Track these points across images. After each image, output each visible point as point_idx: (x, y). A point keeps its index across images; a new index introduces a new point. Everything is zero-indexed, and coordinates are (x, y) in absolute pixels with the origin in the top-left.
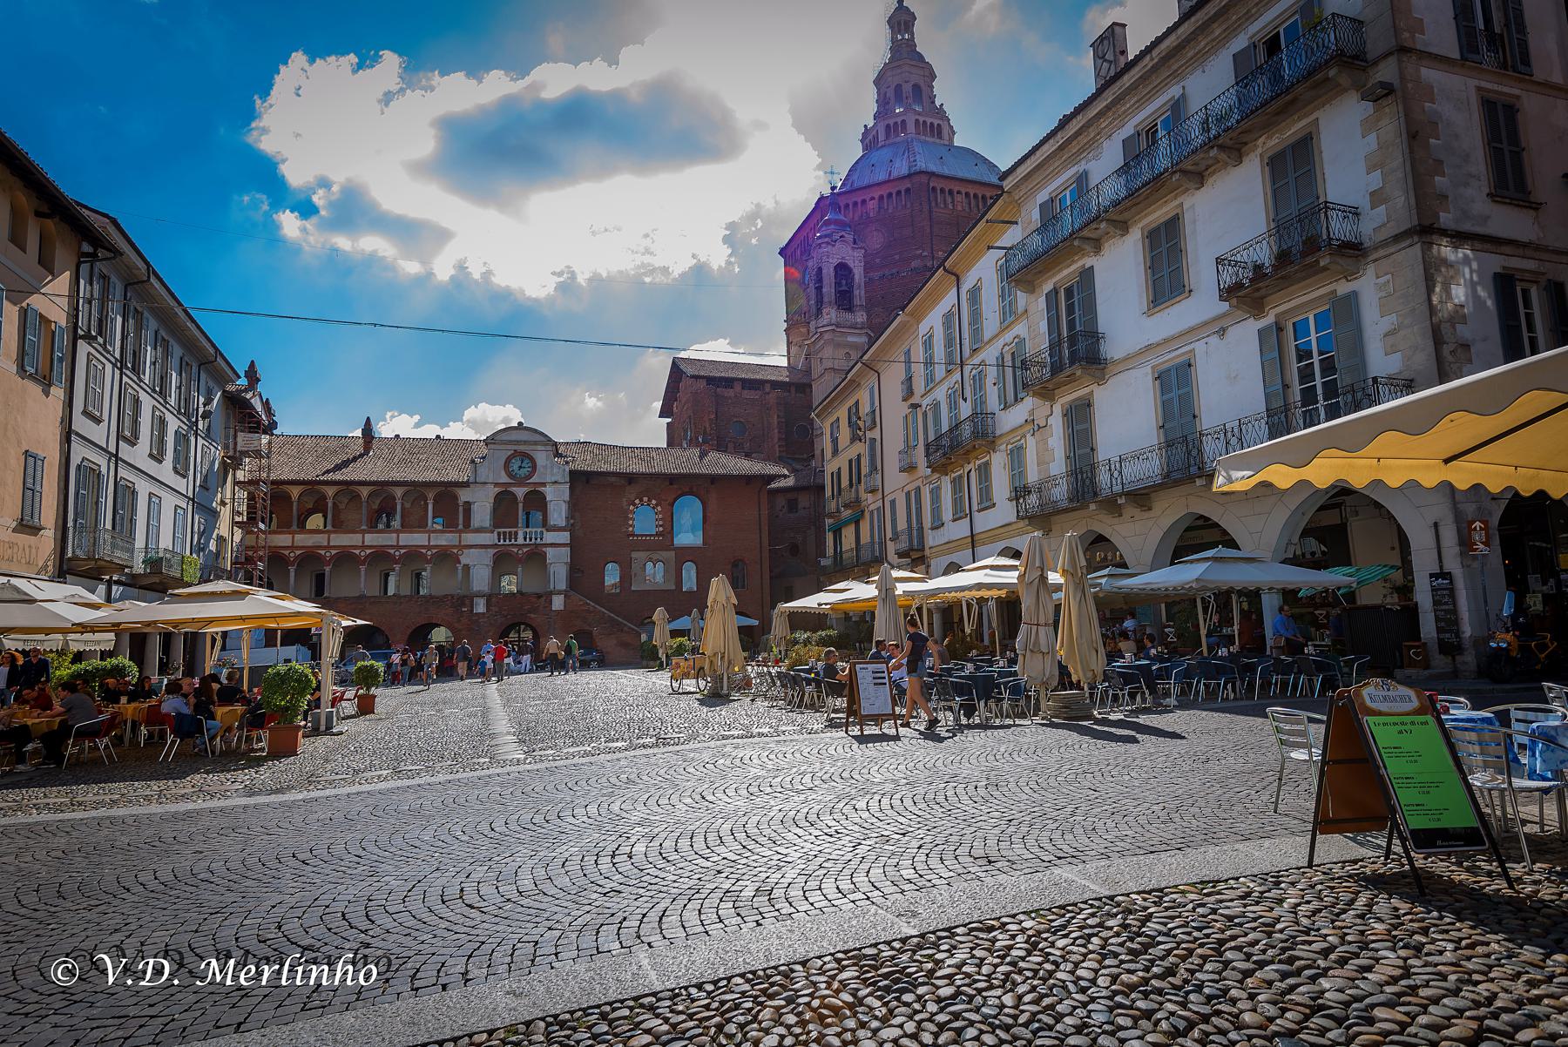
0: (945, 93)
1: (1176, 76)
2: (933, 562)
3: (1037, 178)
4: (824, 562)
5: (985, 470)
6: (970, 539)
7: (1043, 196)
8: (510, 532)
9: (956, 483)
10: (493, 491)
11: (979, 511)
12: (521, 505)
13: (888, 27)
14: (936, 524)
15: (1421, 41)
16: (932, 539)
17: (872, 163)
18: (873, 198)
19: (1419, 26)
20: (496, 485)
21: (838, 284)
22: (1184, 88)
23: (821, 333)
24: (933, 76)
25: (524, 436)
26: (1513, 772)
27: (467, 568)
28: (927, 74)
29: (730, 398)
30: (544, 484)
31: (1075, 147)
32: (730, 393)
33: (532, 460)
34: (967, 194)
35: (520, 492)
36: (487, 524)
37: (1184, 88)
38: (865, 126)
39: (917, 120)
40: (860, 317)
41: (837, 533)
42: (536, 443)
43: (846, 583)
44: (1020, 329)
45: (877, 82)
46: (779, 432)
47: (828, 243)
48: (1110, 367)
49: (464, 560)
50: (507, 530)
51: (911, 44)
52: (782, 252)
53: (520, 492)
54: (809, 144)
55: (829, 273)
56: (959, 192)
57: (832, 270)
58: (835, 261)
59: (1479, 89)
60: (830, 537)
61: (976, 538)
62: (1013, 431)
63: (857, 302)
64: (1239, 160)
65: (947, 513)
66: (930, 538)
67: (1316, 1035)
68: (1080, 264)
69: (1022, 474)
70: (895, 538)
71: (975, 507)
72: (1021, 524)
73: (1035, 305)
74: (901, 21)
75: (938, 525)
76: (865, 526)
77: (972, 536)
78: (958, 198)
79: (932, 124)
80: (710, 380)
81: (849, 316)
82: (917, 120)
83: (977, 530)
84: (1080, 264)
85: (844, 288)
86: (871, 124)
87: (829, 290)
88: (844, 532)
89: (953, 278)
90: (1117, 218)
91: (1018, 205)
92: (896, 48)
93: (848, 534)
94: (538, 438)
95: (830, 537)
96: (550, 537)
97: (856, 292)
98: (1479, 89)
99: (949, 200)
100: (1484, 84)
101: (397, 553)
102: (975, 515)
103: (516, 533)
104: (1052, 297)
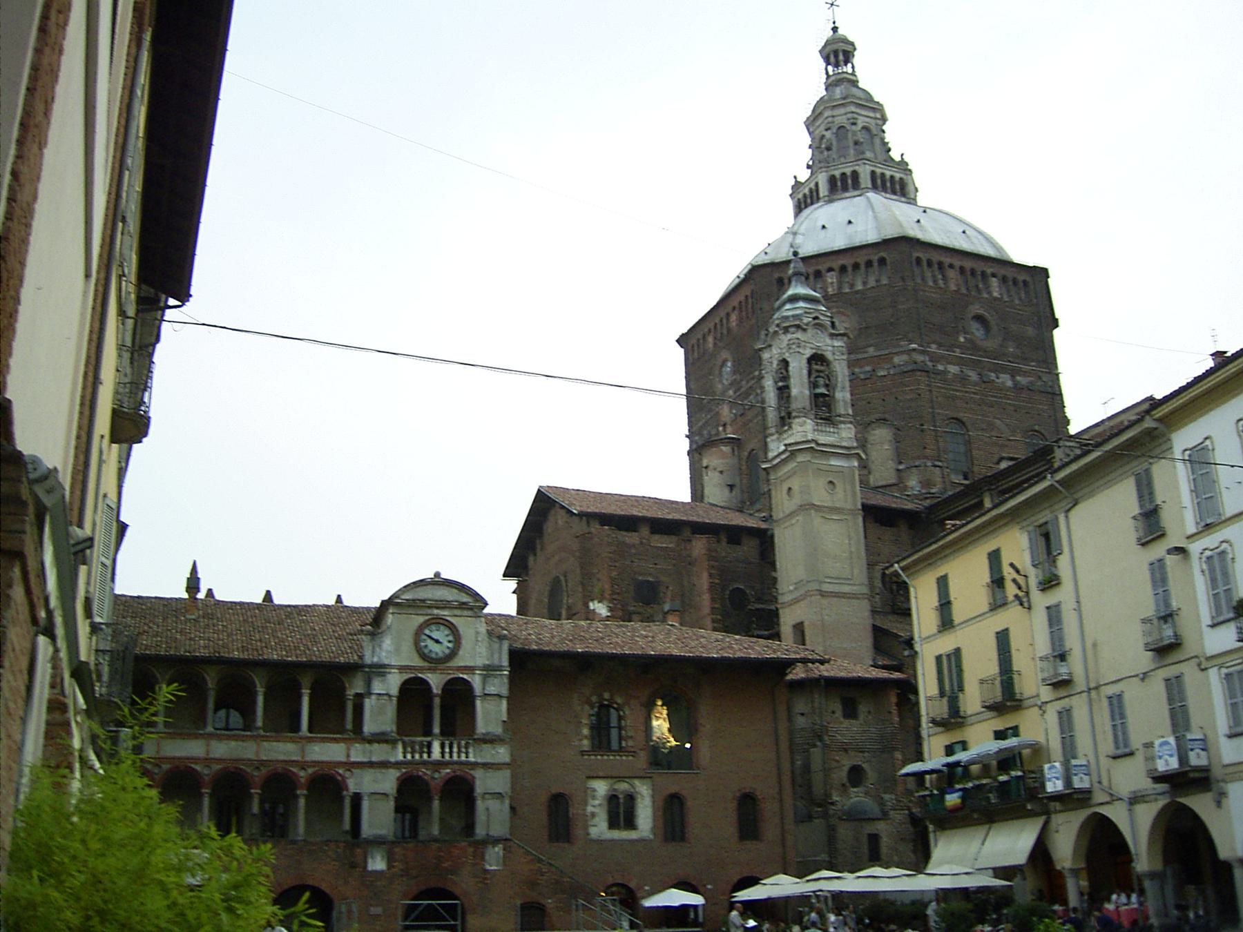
10: (393, 683)
12: (437, 701)
17: (820, 224)
18: (830, 270)
20: (402, 669)
24: (884, 119)
27: (357, 799)
28: (878, 116)
29: (634, 546)
30: (470, 669)
32: (631, 538)
34: (962, 269)
35: (436, 681)
36: (498, 730)
39: (873, 173)
40: (846, 434)
42: (462, 606)
43: (873, 869)
46: (713, 600)
47: (798, 327)
49: (352, 786)
52: (682, 340)
56: (951, 266)
58: (808, 353)
78: (951, 274)
79: (883, 175)
80: (606, 520)
82: (873, 173)
85: (822, 390)
86: (804, 175)
87: (799, 388)
94: (465, 598)
97: (839, 395)
99: (928, 274)
101: (437, 775)
103: (429, 745)
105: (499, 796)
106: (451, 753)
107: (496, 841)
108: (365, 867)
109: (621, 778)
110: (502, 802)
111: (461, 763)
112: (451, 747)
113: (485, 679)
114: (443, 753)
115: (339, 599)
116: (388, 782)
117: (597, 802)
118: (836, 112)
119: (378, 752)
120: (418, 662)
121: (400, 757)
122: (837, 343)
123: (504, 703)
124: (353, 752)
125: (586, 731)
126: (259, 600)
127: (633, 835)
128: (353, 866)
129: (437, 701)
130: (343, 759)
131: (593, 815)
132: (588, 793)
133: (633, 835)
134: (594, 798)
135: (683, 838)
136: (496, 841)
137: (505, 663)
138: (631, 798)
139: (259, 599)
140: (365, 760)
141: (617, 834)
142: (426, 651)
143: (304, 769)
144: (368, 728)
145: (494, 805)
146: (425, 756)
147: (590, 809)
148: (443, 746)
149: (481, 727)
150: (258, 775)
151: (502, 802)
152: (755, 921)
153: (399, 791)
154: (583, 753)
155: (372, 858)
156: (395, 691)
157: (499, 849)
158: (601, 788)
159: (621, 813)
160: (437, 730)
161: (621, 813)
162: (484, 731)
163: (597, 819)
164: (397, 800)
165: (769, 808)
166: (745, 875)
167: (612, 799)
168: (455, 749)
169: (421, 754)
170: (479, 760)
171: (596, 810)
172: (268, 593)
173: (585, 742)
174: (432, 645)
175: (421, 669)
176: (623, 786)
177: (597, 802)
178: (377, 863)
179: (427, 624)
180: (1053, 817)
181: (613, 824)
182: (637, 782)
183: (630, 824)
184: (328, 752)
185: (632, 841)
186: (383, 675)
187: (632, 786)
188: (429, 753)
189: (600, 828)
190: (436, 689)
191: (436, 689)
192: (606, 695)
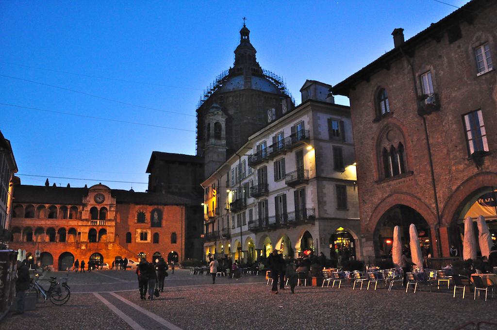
1: (282, 127)
2: (232, 239)
3: (257, 139)
4: (202, 236)
5: (244, 213)
7: (258, 144)
15: (320, 137)
16: (232, 232)
18: (230, 96)
19: (320, 133)
20: (91, 205)
21: (215, 130)
23: (209, 147)
26: (470, 114)
31: (263, 135)
33: (104, 199)
35: (99, 208)
51: (248, 41)
53: (99, 208)
54: (197, 135)
59: (333, 146)
60: (205, 227)
63: (222, 136)
64: (291, 152)
65: (236, 225)
66: (232, 231)
68: (264, 164)
69: (252, 218)
70: (223, 230)
74: (245, 32)
75: (234, 228)
76: (216, 224)
77: (241, 232)
81: (219, 141)
84: (264, 164)
85: (218, 131)
92: (242, 41)
93: (210, 227)
94: (106, 188)
95: (205, 227)
96: (108, 224)
98: (333, 146)
100: (334, 145)
102: (242, 226)
104: (259, 171)
105: (112, 233)
107: (111, 243)
109: (144, 229)
113: (110, 207)
115: (69, 185)
116: (87, 230)
118: (249, 50)
119: (85, 223)
121: (90, 224)
125: (136, 218)
127: (146, 242)
128: (78, 248)
131: (137, 237)
133: (146, 242)
135: (158, 243)
136: (111, 243)
137: (115, 203)
138: (146, 234)
139: (84, 187)
141: (142, 241)
144: (83, 217)
145: (111, 235)
150: (67, 228)
152: (352, 164)
153: (89, 231)
155: (348, 178)
156: (89, 210)
157: (112, 244)
158: (139, 231)
159: (144, 236)
161: (144, 236)
163: (138, 238)
165: (179, 236)
167: (142, 234)
172: (69, 184)
174: (98, 199)
175: (95, 205)
176: (145, 231)
178: (83, 248)
179: (97, 195)
181: (142, 239)
182: (148, 230)
183: (146, 239)
184: (73, 223)
189: (138, 240)
191: (99, 210)
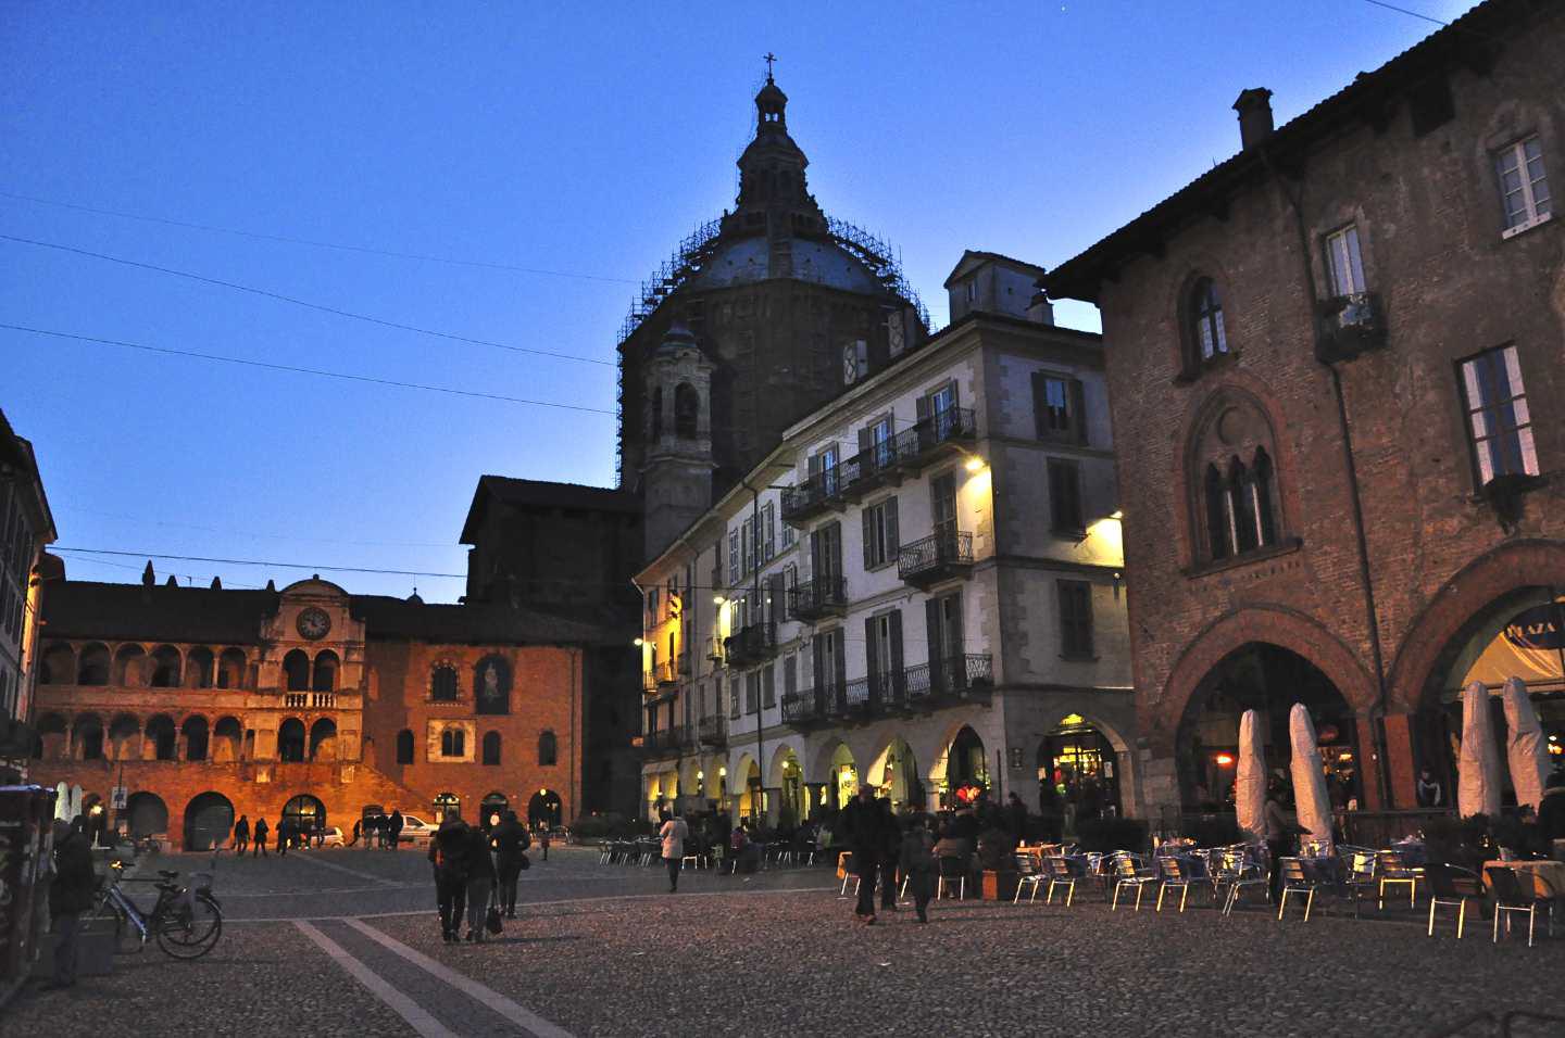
0: (818, 185)
1: (888, 398)
3: (809, 436)
4: (636, 742)
5: (770, 670)
6: (757, 734)
7: (812, 451)
8: (299, 696)
9: (750, 677)
11: (766, 708)
12: (312, 665)
13: (755, 105)
14: (735, 715)
16: (732, 729)
19: (1007, 419)
20: (286, 643)
22: (893, 408)
24: (805, 163)
25: (318, 590)
31: (829, 424)
35: (311, 653)
37: (893, 408)
38: (726, 211)
41: (653, 707)
44: (794, 557)
45: (740, 163)
48: (850, 609)
49: (248, 725)
50: (296, 693)
51: (781, 127)
53: (311, 653)
55: (668, 394)
57: (673, 391)
58: (677, 382)
59: (1048, 458)
61: (763, 732)
62: (788, 643)
63: (700, 428)
64: (918, 477)
65: (744, 709)
67: (303, 595)
70: (703, 722)
71: (762, 705)
72: (784, 727)
73: (803, 538)
74: (771, 101)
75: (736, 717)
76: (679, 705)
77: (760, 730)
83: (764, 726)
84: (831, 517)
85: (686, 413)
88: (659, 709)
89: (752, 493)
90: (856, 491)
91: (795, 451)
92: (763, 128)
95: (646, 713)
98: (1048, 458)
100: (1053, 454)
103: (305, 696)
105: (354, 732)
106: (320, 702)
108: (255, 780)
109: (454, 719)
110: (356, 736)
111: (326, 709)
112: (321, 698)
113: (347, 653)
114: (314, 702)
116: (274, 723)
117: (435, 737)
119: (267, 702)
120: (299, 639)
122: (702, 375)
123: (361, 668)
124: (249, 701)
125: (429, 686)
126: (208, 585)
127: (460, 760)
128: (246, 779)
129: (312, 665)
130: (242, 706)
131: (432, 745)
132: (427, 731)
133: (460, 760)
134: (433, 733)
136: (349, 763)
138: (460, 735)
140: (258, 707)
141: (448, 759)
142: (306, 631)
143: (212, 712)
144: (262, 684)
145: (350, 738)
146: (302, 704)
147: (430, 741)
148: (315, 698)
149: (343, 685)
151: (356, 736)
154: (426, 702)
157: (352, 769)
159: (452, 744)
160: (310, 685)
161: (452, 744)
162: (345, 687)
164: (279, 735)
165: (563, 741)
166: (325, 805)
167: (446, 735)
168: (324, 700)
169: (299, 703)
170: (340, 708)
171: (435, 742)
173: (428, 694)
174: (309, 625)
176: (456, 725)
177: (435, 737)
178: (263, 778)
180: (684, 760)
182: (466, 723)
183: (460, 752)
185: (459, 764)
186: (273, 648)
187: (463, 726)
188: (305, 702)
189: (436, 754)
190: (312, 658)
191: (312, 658)
192: (446, 661)
